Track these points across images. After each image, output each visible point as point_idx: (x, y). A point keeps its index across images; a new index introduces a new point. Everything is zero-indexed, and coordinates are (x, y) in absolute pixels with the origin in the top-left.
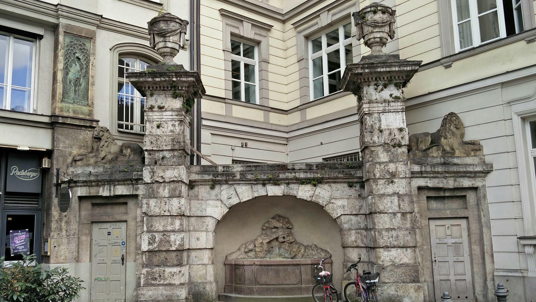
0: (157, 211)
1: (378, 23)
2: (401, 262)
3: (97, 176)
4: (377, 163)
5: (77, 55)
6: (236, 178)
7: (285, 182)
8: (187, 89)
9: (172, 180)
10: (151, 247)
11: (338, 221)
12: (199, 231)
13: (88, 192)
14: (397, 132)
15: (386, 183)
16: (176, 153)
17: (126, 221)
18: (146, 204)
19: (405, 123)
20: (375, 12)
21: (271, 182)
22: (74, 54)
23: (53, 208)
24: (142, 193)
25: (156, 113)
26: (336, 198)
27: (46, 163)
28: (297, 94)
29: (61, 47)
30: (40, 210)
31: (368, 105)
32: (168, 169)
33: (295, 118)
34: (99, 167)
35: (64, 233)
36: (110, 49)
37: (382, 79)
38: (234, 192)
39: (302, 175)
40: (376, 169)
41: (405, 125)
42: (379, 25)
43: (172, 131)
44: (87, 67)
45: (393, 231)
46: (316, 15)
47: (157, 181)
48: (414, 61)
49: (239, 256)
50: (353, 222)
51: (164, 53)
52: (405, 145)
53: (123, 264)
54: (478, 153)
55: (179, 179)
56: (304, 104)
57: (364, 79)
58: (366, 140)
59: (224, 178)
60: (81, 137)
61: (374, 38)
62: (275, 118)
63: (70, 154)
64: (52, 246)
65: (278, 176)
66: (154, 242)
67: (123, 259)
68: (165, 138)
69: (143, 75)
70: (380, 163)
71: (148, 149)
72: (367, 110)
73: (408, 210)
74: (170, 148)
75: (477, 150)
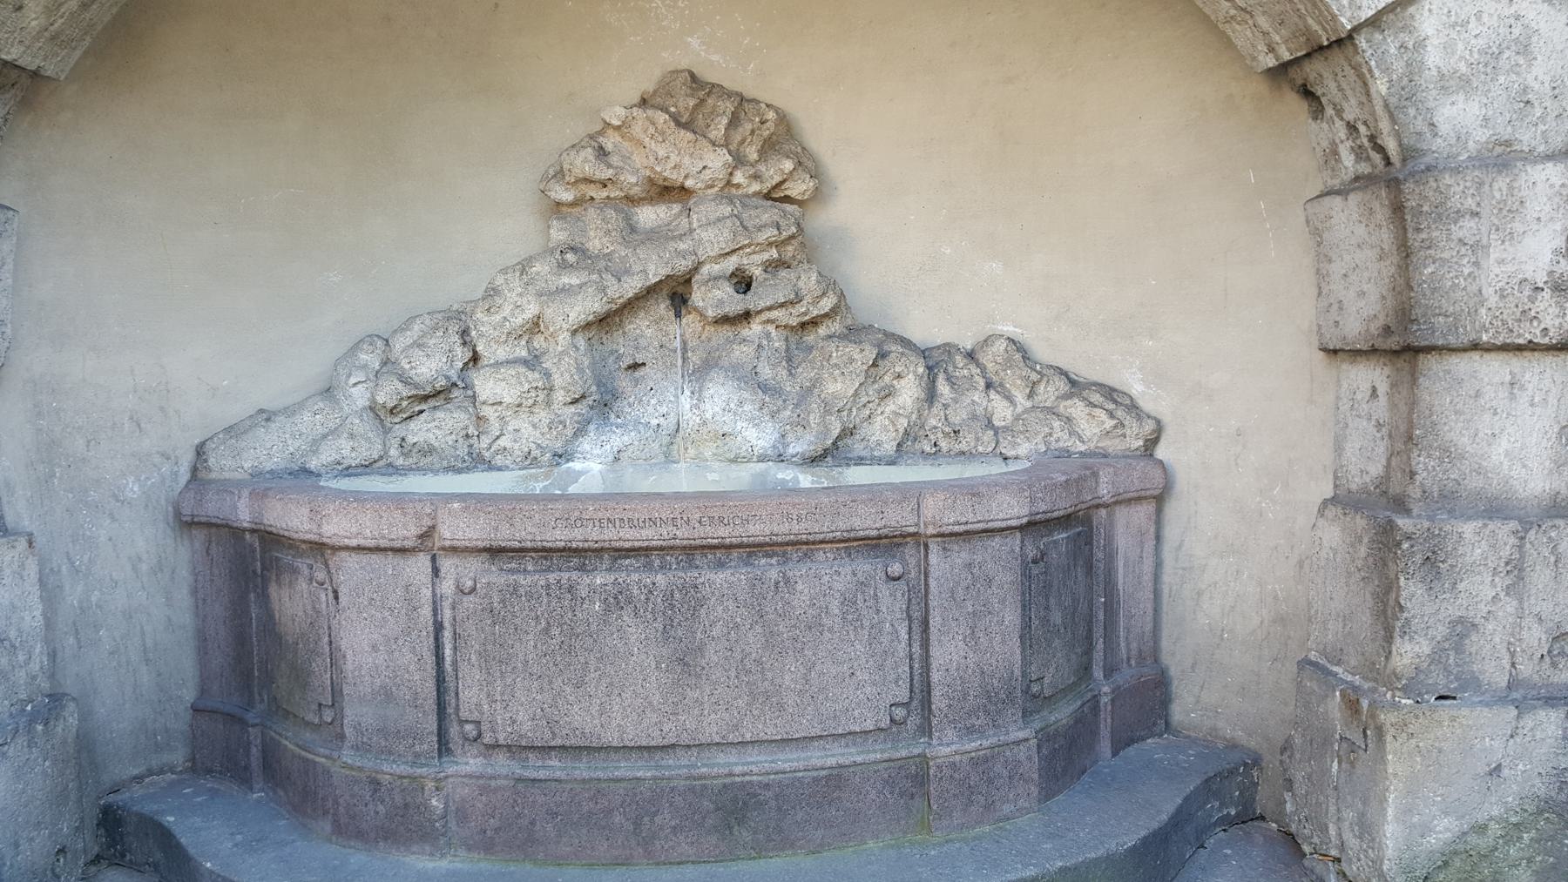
49: (315, 445)
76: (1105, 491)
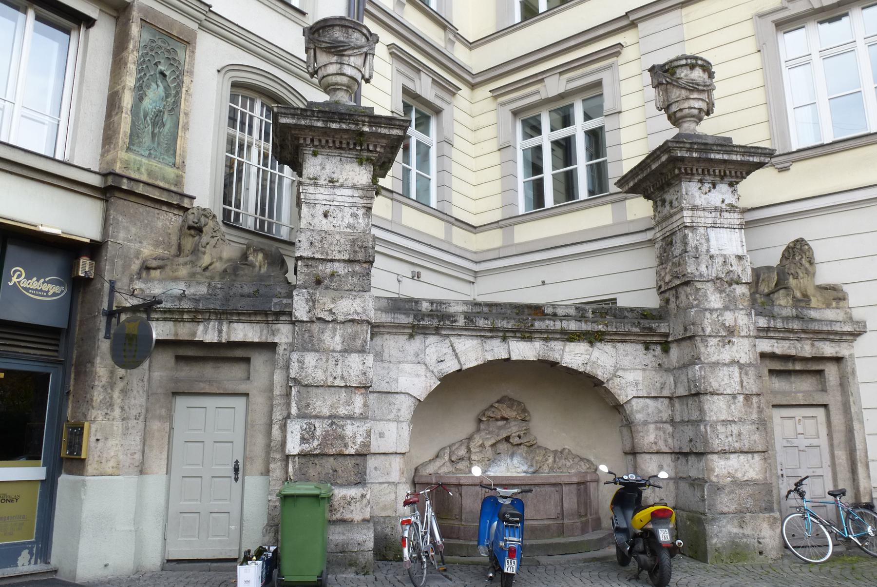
0: (320, 376)
1: (698, 85)
2: (746, 478)
3: (196, 301)
4: (706, 310)
5: (161, 67)
6: (457, 324)
7: (542, 336)
8: (382, 151)
9: (350, 317)
10: (306, 447)
11: (627, 407)
12: (382, 420)
13: (173, 331)
14: (734, 261)
15: (721, 344)
16: (357, 268)
17: (247, 395)
18: (299, 361)
19: (745, 248)
20: (692, 67)
21: (518, 335)
22: (156, 64)
23: (98, 360)
24: (286, 340)
25: (322, 190)
26: (625, 369)
27: (85, 267)
28: (497, 202)
29: (134, 47)
30: (60, 363)
31: (690, 213)
32: (342, 298)
33: (493, 240)
34: (199, 283)
35: (117, 412)
36: (219, 71)
37: (712, 173)
38: (450, 351)
39: (573, 326)
40: (706, 320)
41: (745, 251)
42: (701, 88)
43: (349, 226)
44: (178, 94)
45: (733, 425)
46: (539, 79)
47: (319, 319)
48: (765, 149)
50: (650, 410)
51: (336, 84)
52: (746, 283)
53: (236, 479)
54: (841, 303)
55: (364, 318)
56: (511, 218)
57: (686, 169)
58: (689, 271)
59: (435, 322)
60: (160, 224)
61: (690, 108)
62: (460, 238)
63: (138, 254)
64: (93, 439)
65: (532, 325)
66: (313, 437)
67: (236, 470)
68: (338, 237)
69: (309, 113)
70: (711, 311)
71: (305, 254)
72: (688, 220)
73: (755, 390)
74: (346, 257)
75: (840, 299)
76: (589, 479)
